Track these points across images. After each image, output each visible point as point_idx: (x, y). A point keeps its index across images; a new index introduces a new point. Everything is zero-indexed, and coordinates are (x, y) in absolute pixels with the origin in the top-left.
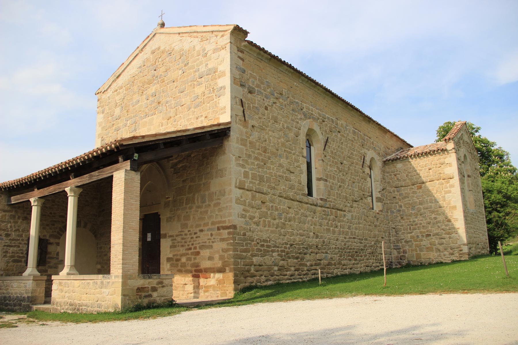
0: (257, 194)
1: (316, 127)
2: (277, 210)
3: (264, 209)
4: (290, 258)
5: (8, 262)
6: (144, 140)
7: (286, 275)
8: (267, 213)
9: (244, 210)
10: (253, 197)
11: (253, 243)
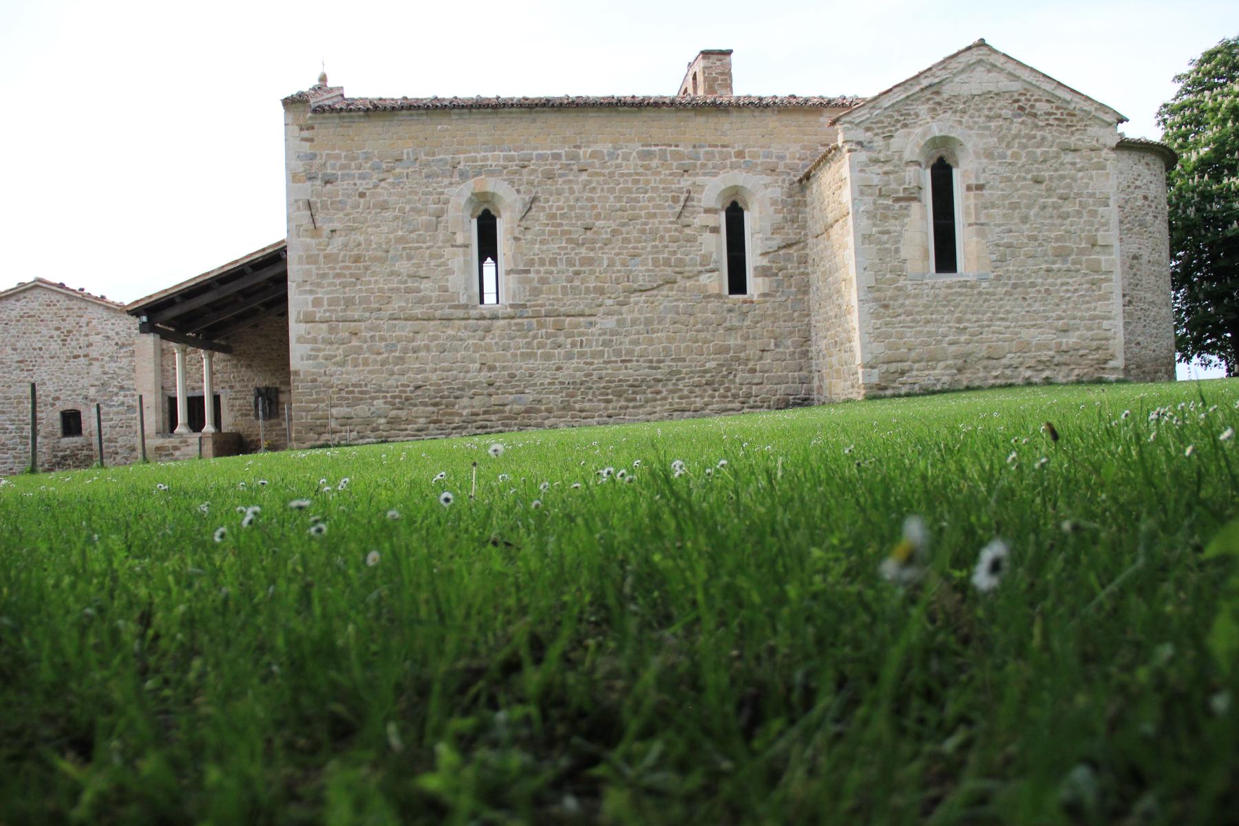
0: (341, 324)
1: (493, 185)
2: (382, 339)
3: (355, 343)
4: (415, 405)
5: (236, 417)
6: (152, 300)
7: (406, 430)
8: (361, 348)
9: (312, 349)
10: (332, 330)
11: (331, 390)
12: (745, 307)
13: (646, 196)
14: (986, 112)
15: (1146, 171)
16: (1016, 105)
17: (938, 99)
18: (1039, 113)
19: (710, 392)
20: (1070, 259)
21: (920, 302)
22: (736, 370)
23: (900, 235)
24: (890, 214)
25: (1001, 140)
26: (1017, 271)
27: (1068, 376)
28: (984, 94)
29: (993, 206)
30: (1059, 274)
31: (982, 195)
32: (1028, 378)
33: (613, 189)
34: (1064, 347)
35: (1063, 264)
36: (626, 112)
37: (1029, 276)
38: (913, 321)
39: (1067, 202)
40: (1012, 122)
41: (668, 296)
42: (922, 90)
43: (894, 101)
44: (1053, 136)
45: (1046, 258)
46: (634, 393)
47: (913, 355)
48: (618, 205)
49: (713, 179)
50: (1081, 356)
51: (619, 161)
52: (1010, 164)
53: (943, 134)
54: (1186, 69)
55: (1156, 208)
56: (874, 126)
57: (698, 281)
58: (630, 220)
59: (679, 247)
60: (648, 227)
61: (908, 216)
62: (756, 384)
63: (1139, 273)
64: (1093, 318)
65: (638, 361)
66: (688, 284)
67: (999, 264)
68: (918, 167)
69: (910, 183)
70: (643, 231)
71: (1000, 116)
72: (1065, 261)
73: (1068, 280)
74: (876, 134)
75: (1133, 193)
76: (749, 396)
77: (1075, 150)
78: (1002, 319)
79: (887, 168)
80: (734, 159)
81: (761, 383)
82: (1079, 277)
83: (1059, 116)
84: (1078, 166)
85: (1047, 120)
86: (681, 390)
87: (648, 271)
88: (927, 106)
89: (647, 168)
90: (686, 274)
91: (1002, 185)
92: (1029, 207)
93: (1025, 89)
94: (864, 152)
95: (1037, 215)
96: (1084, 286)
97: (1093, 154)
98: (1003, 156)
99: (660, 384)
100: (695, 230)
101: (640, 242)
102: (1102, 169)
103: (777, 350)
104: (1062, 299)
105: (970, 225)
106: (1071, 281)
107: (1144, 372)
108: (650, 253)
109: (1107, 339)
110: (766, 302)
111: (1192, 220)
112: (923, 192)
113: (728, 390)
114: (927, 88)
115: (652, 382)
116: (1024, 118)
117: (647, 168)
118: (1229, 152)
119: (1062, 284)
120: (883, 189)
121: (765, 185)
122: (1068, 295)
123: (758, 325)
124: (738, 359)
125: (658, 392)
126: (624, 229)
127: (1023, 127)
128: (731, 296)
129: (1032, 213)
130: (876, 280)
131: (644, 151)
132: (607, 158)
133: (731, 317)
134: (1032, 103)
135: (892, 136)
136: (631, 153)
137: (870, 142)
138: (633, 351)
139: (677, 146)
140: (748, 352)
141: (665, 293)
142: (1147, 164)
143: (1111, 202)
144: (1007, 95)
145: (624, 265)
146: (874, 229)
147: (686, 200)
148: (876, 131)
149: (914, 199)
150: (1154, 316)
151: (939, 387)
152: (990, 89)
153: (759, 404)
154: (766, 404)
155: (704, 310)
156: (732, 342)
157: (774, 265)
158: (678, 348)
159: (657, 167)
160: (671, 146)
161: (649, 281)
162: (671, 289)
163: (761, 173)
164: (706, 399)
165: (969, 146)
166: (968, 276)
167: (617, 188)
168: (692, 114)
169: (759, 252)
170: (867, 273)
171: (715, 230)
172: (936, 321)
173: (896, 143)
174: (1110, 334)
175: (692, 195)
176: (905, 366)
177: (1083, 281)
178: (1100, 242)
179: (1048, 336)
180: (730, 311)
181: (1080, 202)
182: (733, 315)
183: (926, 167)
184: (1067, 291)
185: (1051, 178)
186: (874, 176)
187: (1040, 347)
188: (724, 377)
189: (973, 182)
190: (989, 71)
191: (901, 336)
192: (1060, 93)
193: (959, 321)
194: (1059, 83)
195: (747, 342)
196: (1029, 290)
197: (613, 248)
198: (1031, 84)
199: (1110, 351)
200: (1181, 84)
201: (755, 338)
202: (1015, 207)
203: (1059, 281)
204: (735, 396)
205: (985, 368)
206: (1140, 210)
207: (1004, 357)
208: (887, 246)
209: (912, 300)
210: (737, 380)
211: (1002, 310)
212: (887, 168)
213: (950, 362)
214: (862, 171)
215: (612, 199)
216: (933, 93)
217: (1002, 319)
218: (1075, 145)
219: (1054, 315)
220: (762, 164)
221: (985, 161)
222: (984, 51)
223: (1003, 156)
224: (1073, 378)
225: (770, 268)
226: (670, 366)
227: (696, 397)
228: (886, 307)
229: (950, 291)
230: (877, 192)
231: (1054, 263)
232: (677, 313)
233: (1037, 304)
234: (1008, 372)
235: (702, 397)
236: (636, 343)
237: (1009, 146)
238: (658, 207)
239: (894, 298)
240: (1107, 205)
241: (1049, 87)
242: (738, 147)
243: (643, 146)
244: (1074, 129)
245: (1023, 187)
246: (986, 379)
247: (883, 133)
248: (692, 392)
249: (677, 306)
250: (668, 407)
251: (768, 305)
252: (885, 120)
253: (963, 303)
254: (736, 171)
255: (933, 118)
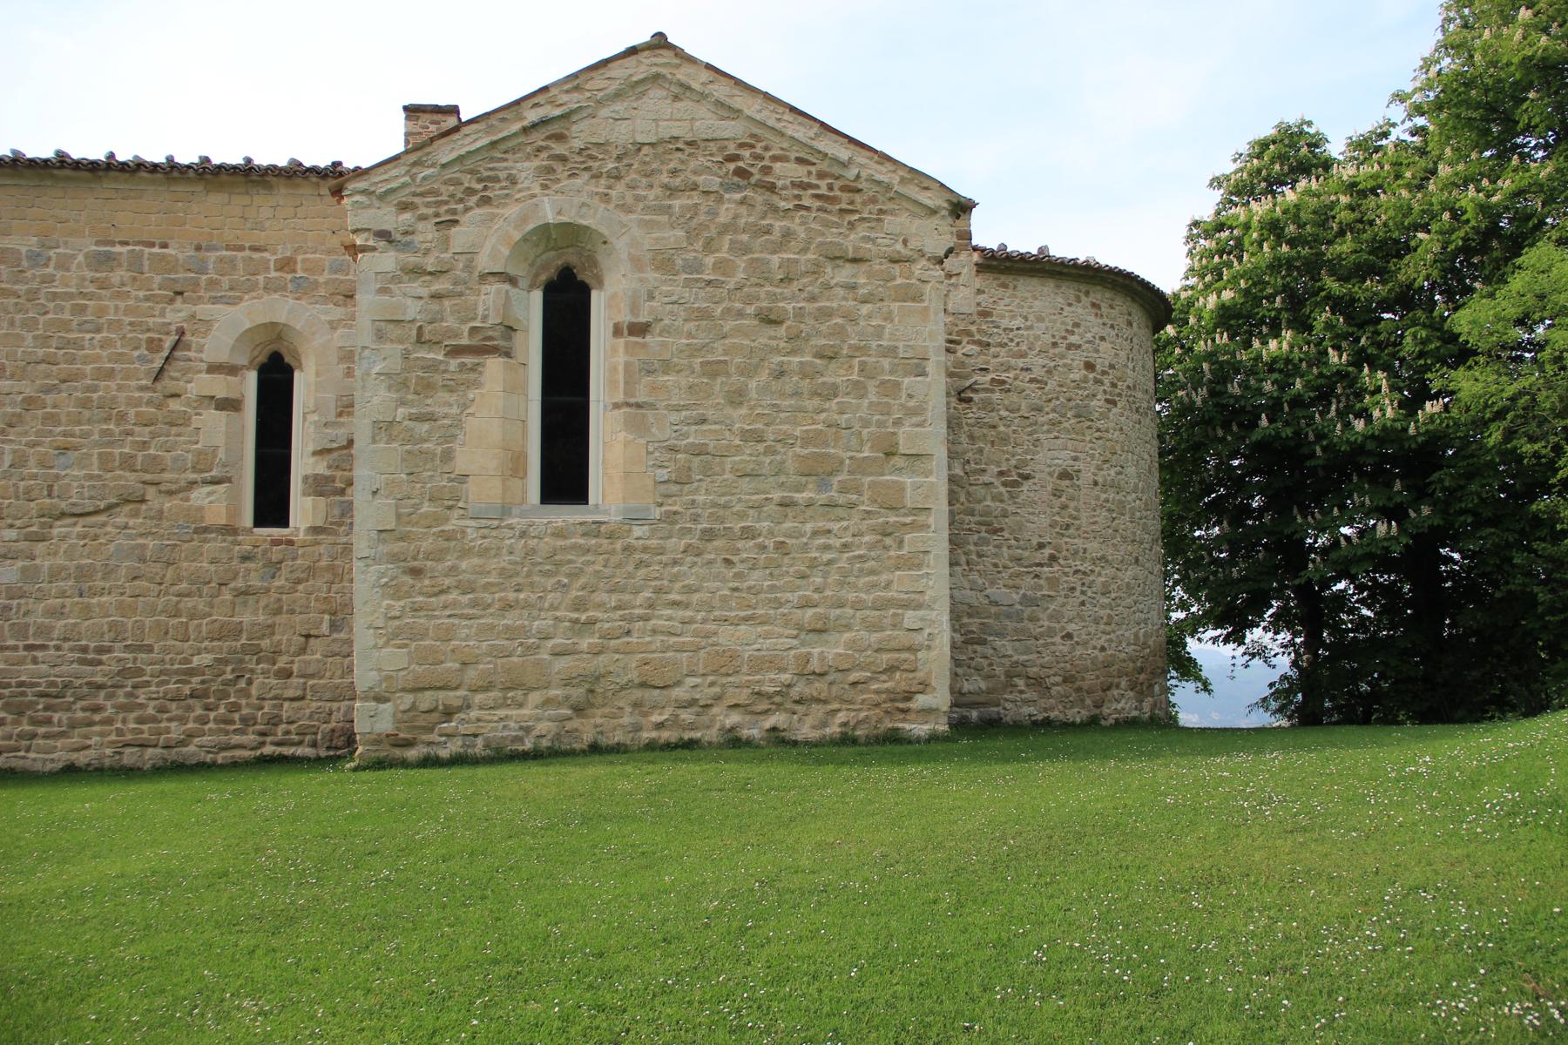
12: (276, 553)
13: (98, 337)
14: (665, 179)
15: (1092, 318)
16: (732, 166)
17: (559, 149)
18: (780, 183)
19: (199, 712)
20: (835, 480)
21: (493, 564)
22: (252, 671)
23: (458, 424)
24: (438, 378)
25: (691, 236)
26: (715, 505)
27: (824, 724)
28: (661, 142)
29: (667, 367)
30: (809, 512)
31: (644, 346)
32: (732, 729)
33: (36, 321)
34: (815, 665)
35: (819, 491)
36: (68, 179)
37: (741, 516)
38: (474, 604)
39: (833, 365)
40: (720, 200)
41: (126, 527)
42: (525, 130)
43: (462, 152)
44: (809, 230)
45: (782, 478)
46: (46, 709)
47: (472, 674)
48: (41, 352)
49: (230, 309)
50: (854, 684)
51: (50, 270)
52: (709, 283)
53: (564, 219)
54: (1229, 168)
55: (1114, 385)
56: (417, 200)
57: (187, 499)
58: (64, 381)
59: (154, 435)
60: (95, 396)
61: (477, 384)
62: (292, 700)
63: (1072, 504)
64: (880, 606)
65: (58, 648)
66: (167, 505)
67: (674, 488)
68: (507, 286)
69: (485, 318)
70: (85, 404)
71: (695, 187)
72: (823, 486)
73: (830, 525)
74: (423, 218)
75: (1063, 357)
76: (274, 721)
77: (855, 261)
78: (675, 604)
79: (440, 285)
80: (273, 274)
81: (302, 698)
82: (856, 518)
83: (823, 191)
84: (862, 291)
85: (798, 197)
86: (141, 706)
87: (91, 477)
88: (536, 163)
89: (103, 285)
90: (163, 488)
91: (691, 325)
92: (748, 371)
93: (753, 136)
94: (392, 254)
95: (764, 390)
96: (866, 539)
97: (897, 268)
98: (695, 267)
99: (102, 693)
100: (189, 405)
101: (79, 423)
102: (913, 300)
103: (335, 636)
104: (814, 562)
105: (616, 406)
106: (835, 526)
107: (1079, 689)
108: (97, 444)
109: (911, 649)
110: (317, 543)
111: (1199, 409)
112: (518, 338)
113: (235, 707)
114: (534, 126)
115: (85, 689)
116: (748, 193)
117: (103, 285)
118: (1267, 298)
119: (815, 533)
120: (427, 329)
121: (330, 322)
122: (827, 556)
123: (301, 587)
124: (257, 651)
125: (97, 709)
126: (49, 399)
127: (743, 210)
128: (257, 530)
129: (753, 384)
130: (399, 516)
131: (99, 253)
132: (25, 264)
133: (248, 571)
134: (766, 163)
135: (457, 222)
136: (73, 257)
137: (406, 233)
138: (51, 628)
139: (165, 246)
140: (277, 637)
141: (121, 520)
142: (1094, 305)
143: (930, 367)
144: (713, 147)
145: (42, 464)
146: (401, 410)
147: (174, 348)
148: (424, 210)
149: (493, 350)
150: (1104, 584)
151: (528, 745)
152: (676, 133)
153: (294, 737)
154: (307, 738)
155: (195, 555)
156: (246, 618)
157: (339, 474)
158: (141, 627)
159: (123, 285)
160: (152, 245)
161: (91, 498)
162: (136, 514)
163: (325, 300)
164: (190, 725)
165: (621, 245)
166: (606, 512)
167: (42, 319)
168: (199, 188)
169: (311, 448)
170: (379, 501)
171: (230, 405)
172: (528, 605)
173: (461, 237)
174: (919, 638)
175: (188, 337)
176: (453, 698)
177: (864, 527)
178: (902, 450)
179: (780, 641)
180: (245, 558)
181: (863, 365)
182: (251, 565)
183: (532, 286)
184: (827, 548)
185: (800, 314)
186: (409, 301)
187: (758, 665)
188: (226, 683)
189: (625, 318)
190: (676, 98)
191: (447, 635)
192: (826, 145)
193: (579, 606)
194: (823, 124)
195: (278, 619)
196: (740, 544)
197: (26, 433)
198: (763, 124)
199: (920, 675)
200: (1222, 191)
201: (292, 612)
202: (714, 370)
203: (809, 527)
204: (247, 721)
205: (636, 705)
206: (1078, 387)
207: (678, 683)
208: (425, 446)
209: (476, 561)
210: (254, 691)
211: (678, 585)
212: (440, 285)
213: (555, 692)
214: (383, 290)
215: (29, 340)
216: (549, 138)
217: (675, 604)
218: (856, 249)
219: (794, 597)
220: (326, 283)
221: (652, 276)
222: (667, 56)
223: (695, 267)
224: (834, 729)
225: (332, 479)
226: (120, 660)
227: (170, 720)
228: (416, 572)
229: (560, 543)
230: (414, 332)
231: (799, 488)
232: (143, 560)
233: (756, 574)
234: (687, 716)
235: (182, 720)
236: (58, 613)
237: (709, 246)
238: (119, 358)
239: (439, 555)
240: (923, 374)
241: (801, 132)
242: (284, 252)
243: (98, 243)
244: (857, 217)
245: (737, 330)
246: (637, 728)
247: (437, 215)
248: (162, 710)
249: (144, 546)
250: (113, 737)
251: (322, 549)
252: (443, 189)
253: (590, 569)
254: (276, 296)
255: (544, 187)
